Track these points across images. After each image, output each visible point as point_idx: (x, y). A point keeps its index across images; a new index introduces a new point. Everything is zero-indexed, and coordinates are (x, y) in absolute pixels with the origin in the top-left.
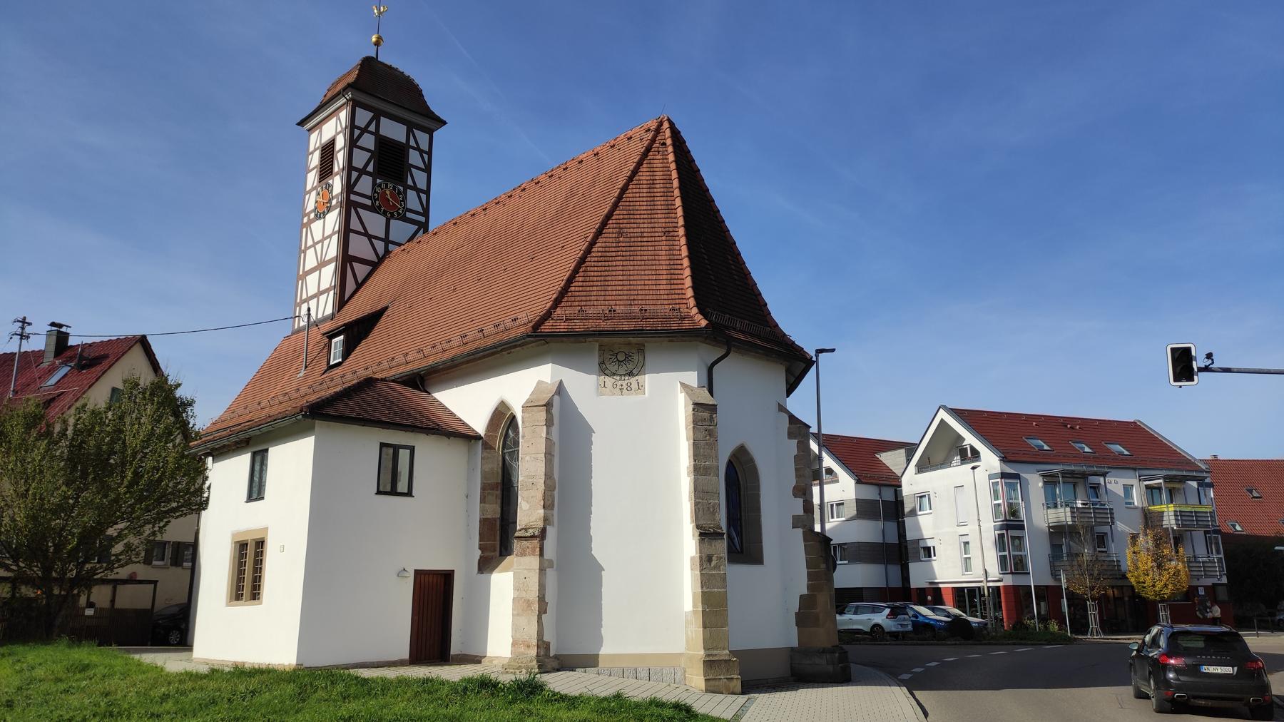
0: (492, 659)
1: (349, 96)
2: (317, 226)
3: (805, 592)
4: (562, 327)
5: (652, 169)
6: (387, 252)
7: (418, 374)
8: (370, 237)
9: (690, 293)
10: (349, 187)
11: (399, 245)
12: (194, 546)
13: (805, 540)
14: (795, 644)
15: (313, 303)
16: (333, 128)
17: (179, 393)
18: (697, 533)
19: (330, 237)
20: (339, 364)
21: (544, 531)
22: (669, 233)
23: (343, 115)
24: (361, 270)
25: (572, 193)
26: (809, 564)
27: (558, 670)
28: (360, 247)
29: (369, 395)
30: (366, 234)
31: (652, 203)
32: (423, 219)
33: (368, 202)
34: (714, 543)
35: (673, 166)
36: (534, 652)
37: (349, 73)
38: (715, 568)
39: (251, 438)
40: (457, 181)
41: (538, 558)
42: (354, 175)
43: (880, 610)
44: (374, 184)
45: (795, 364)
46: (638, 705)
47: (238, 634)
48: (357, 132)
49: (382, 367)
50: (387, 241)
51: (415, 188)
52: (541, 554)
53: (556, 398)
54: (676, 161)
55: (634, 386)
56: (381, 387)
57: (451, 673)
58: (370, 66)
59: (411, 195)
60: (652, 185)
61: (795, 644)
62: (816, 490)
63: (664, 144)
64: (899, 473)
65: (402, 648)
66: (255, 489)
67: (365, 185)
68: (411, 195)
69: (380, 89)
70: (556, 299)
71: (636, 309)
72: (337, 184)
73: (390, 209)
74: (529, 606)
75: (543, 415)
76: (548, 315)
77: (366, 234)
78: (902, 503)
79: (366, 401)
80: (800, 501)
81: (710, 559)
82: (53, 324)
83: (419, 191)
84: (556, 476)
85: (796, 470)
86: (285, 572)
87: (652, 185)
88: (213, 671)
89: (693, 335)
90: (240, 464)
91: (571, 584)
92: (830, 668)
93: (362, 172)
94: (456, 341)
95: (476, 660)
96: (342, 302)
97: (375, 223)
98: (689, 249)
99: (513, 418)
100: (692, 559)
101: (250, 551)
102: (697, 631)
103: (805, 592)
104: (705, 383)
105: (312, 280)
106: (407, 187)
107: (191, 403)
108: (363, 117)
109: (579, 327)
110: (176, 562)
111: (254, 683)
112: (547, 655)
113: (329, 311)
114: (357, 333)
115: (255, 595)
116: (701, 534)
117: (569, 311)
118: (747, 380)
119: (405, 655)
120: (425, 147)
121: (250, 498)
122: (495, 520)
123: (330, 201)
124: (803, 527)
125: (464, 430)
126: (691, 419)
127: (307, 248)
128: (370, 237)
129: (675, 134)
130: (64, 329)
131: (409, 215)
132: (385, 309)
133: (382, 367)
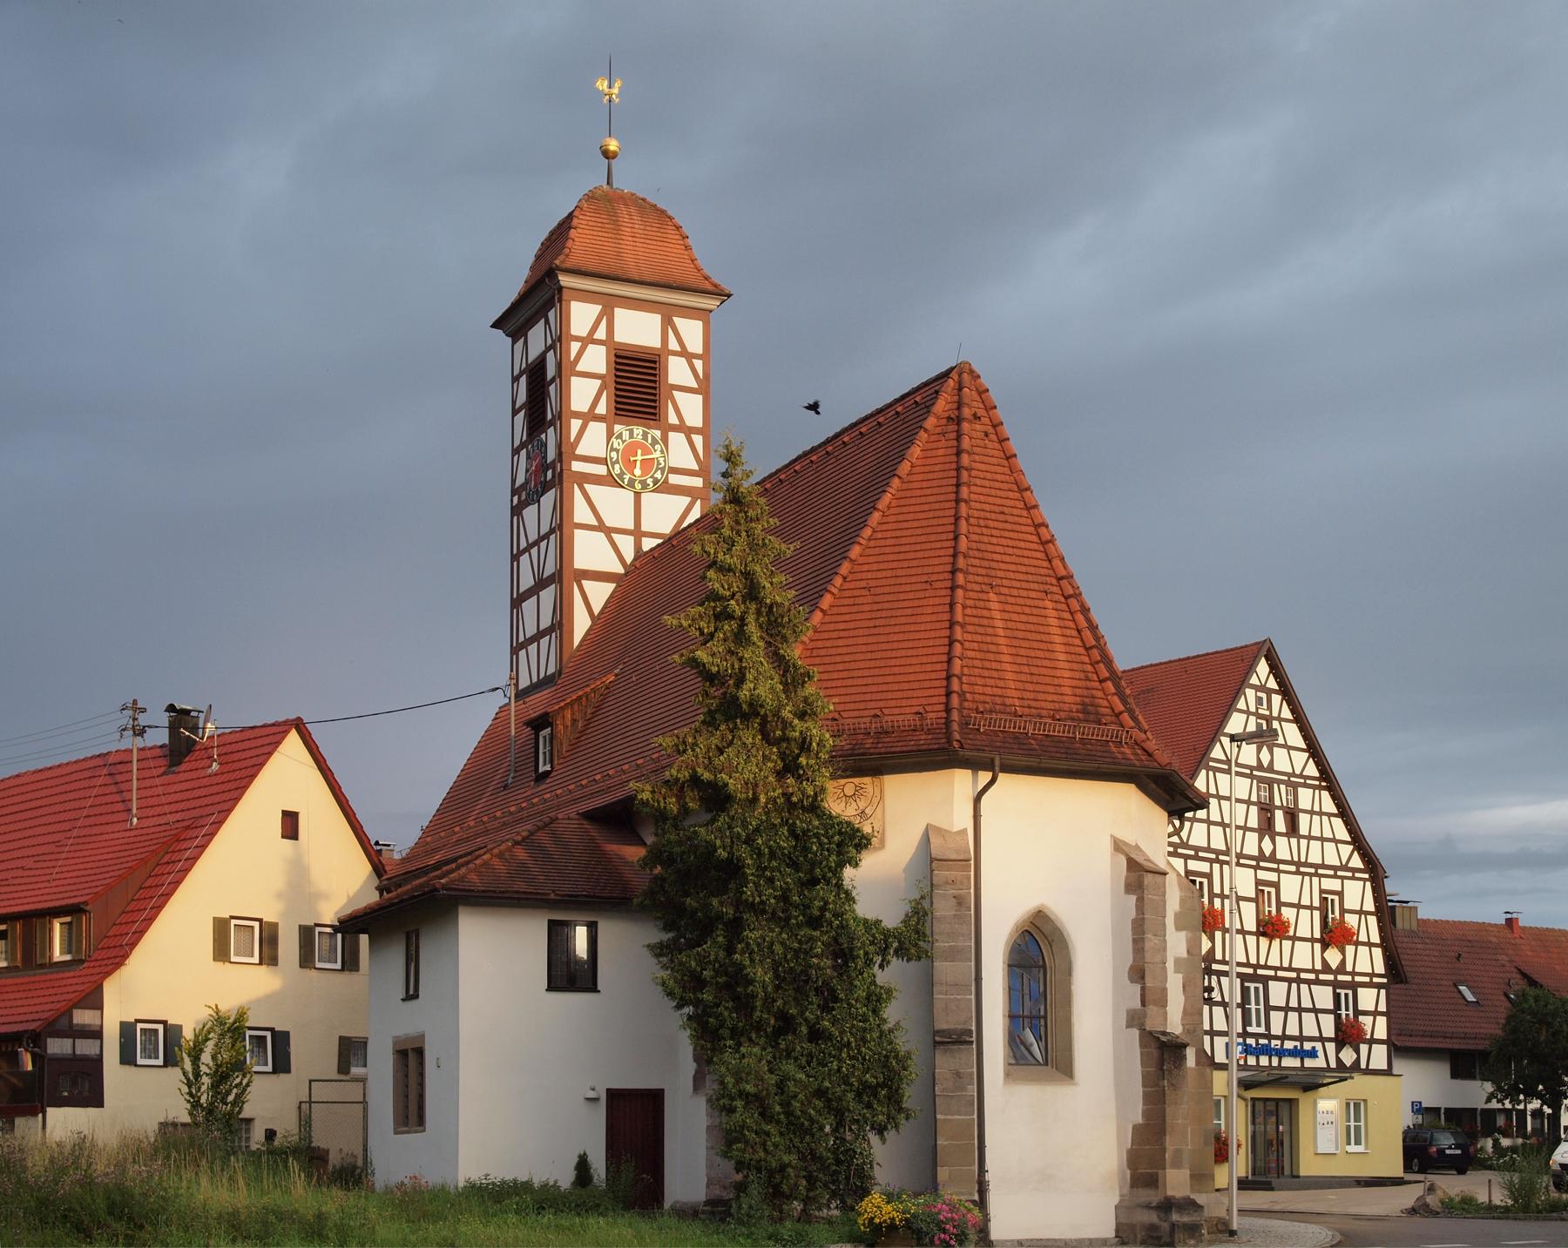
8: (608, 531)
13: (1142, 1046)
30: (601, 527)
44: (610, 434)
106: (667, 429)
115: (421, 1121)
131: (675, 479)
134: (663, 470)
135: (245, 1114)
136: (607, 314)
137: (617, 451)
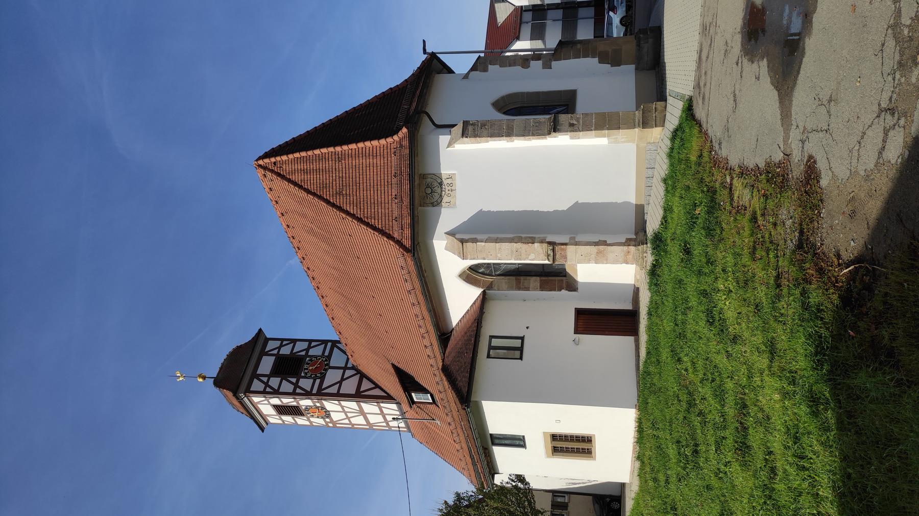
0: (637, 280)
1: (242, 395)
2: (335, 417)
3: (596, 59)
4: (407, 232)
5: (293, 172)
6: (353, 368)
7: (439, 337)
8: (343, 379)
9: (383, 141)
10: (308, 394)
11: (348, 359)
12: (555, 493)
15: (389, 418)
16: (266, 406)
17: (451, 503)
18: (553, 134)
19: (342, 407)
20: (432, 396)
21: (550, 243)
22: (340, 158)
23: (256, 399)
24: (366, 385)
25: (311, 231)
26: (577, 56)
27: (645, 232)
28: (350, 386)
29: (454, 368)
30: (340, 383)
31: (318, 171)
32: (329, 344)
33: (318, 381)
34: (561, 122)
35: (291, 156)
36: (632, 248)
37: (226, 396)
38: (578, 121)
39: (482, 446)
40: (303, 319)
42: (298, 391)
43: (610, 18)
45: (433, 66)
46: (672, 165)
47: (614, 461)
48: (268, 389)
49: (434, 364)
50: (345, 368)
51: (307, 350)
53: (458, 236)
54: (287, 154)
55: (449, 181)
56: (447, 362)
57: (645, 298)
58: (219, 382)
59: (312, 352)
60: (305, 171)
61: (633, 67)
63: (275, 163)
64: (512, 9)
65: (627, 341)
66: (517, 442)
67: (306, 383)
68: (312, 352)
69: (237, 374)
70: (388, 238)
71: (394, 180)
72: (305, 403)
73: (322, 367)
75: (469, 245)
76: (399, 243)
77: (340, 383)
78: (534, 6)
79: (462, 363)
80: (533, 63)
81: (572, 125)
83: (310, 347)
84: (512, 236)
86: (573, 419)
87: (305, 171)
88: (638, 458)
89: (413, 139)
90: (500, 454)
91: (586, 225)
92: (651, 41)
93: (296, 385)
94: (417, 310)
95: (636, 291)
96: (389, 398)
97: (332, 376)
98: (351, 143)
99: (473, 269)
100: (572, 138)
101: (559, 444)
102: (622, 134)
103: (596, 59)
104: (447, 130)
105: (373, 419)
107: (458, 495)
108: (257, 385)
109: (407, 220)
110: (564, 506)
111: (646, 425)
112: (635, 240)
113: (394, 406)
114: (409, 384)
115: (588, 440)
116: (555, 131)
117: (395, 228)
118: (445, 101)
119: (631, 339)
120: (278, 343)
121: (523, 446)
122: (541, 281)
123: (317, 407)
124: (551, 60)
125: (479, 303)
126: (473, 139)
127: (351, 423)
128: (343, 379)
129: (267, 155)
131: (327, 354)
132: (393, 366)
133: (434, 364)
135: (760, 7)
136: (258, 377)
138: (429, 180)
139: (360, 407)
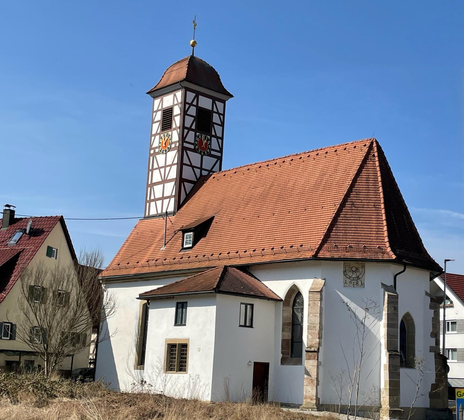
2: (161, 158)
4: (328, 255)
8: (193, 167)
9: (386, 239)
10: (183, 138)
14: (429, 407)
18: (388, 354)
19: (171, 166)
21: (319, 349)
28: (188, 173)
30: (191, 165)
32: (219, 154)
33: (192, 147)
35: (378, 169)
36: (314, 402)
41: (316, 361)
42: (186, 131)
51: (216, 136)
52: (318, 359)
59: (214, 139)
62: (441, 311)
63: (374, 155)
67: (191, 137)
68: (214, 139)
72: (175, 136)
73: (202, 149)
74: (312, 382)
82: (7, 206)
84: (323, 324)
85: (433, 324)
93: (190, 129)
97: (195, 158)
99: (299, 294)
100: (385, 365)
114: (201, 230)
121: (176, 324)
122: (289, 340)
124: (435, 352)
127: (153, 169)
128: (193, 167)
129: (379, 148)
130: (12, 208)
131: (213, 153)
134: (210, 149)
136: (197, 97)
137: (197, 141)
138: (361, 270)
139: (171, 181)
